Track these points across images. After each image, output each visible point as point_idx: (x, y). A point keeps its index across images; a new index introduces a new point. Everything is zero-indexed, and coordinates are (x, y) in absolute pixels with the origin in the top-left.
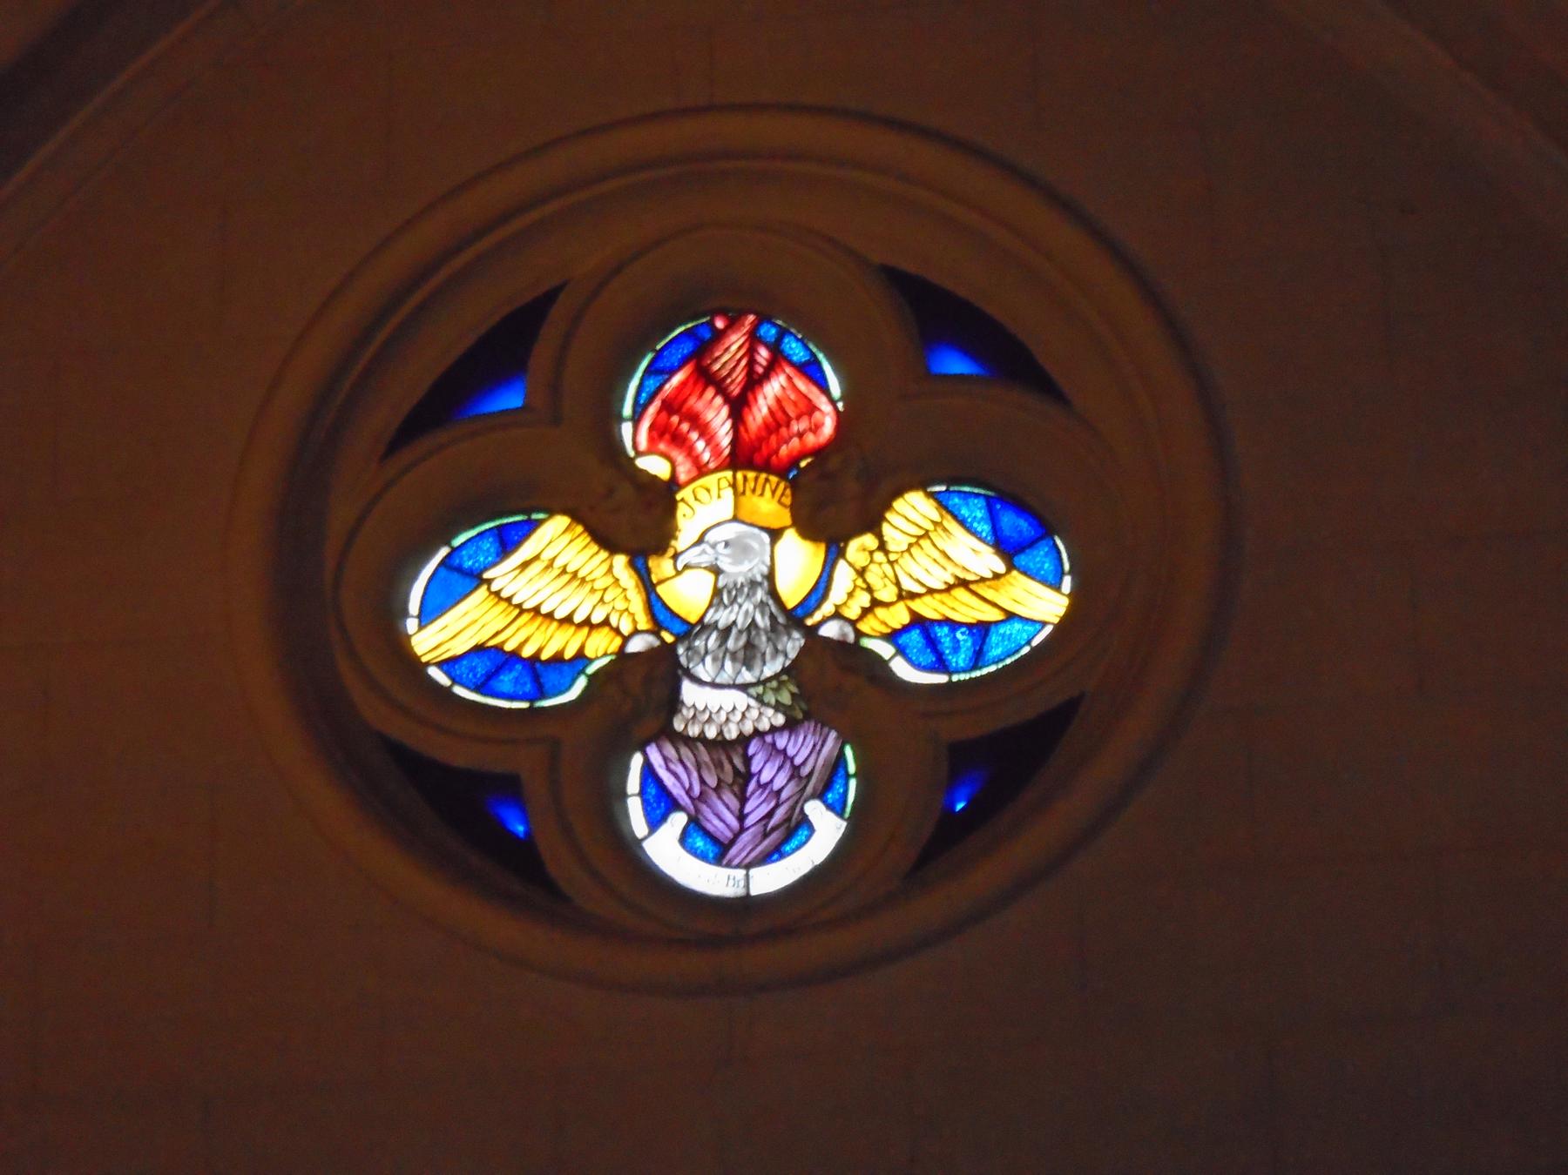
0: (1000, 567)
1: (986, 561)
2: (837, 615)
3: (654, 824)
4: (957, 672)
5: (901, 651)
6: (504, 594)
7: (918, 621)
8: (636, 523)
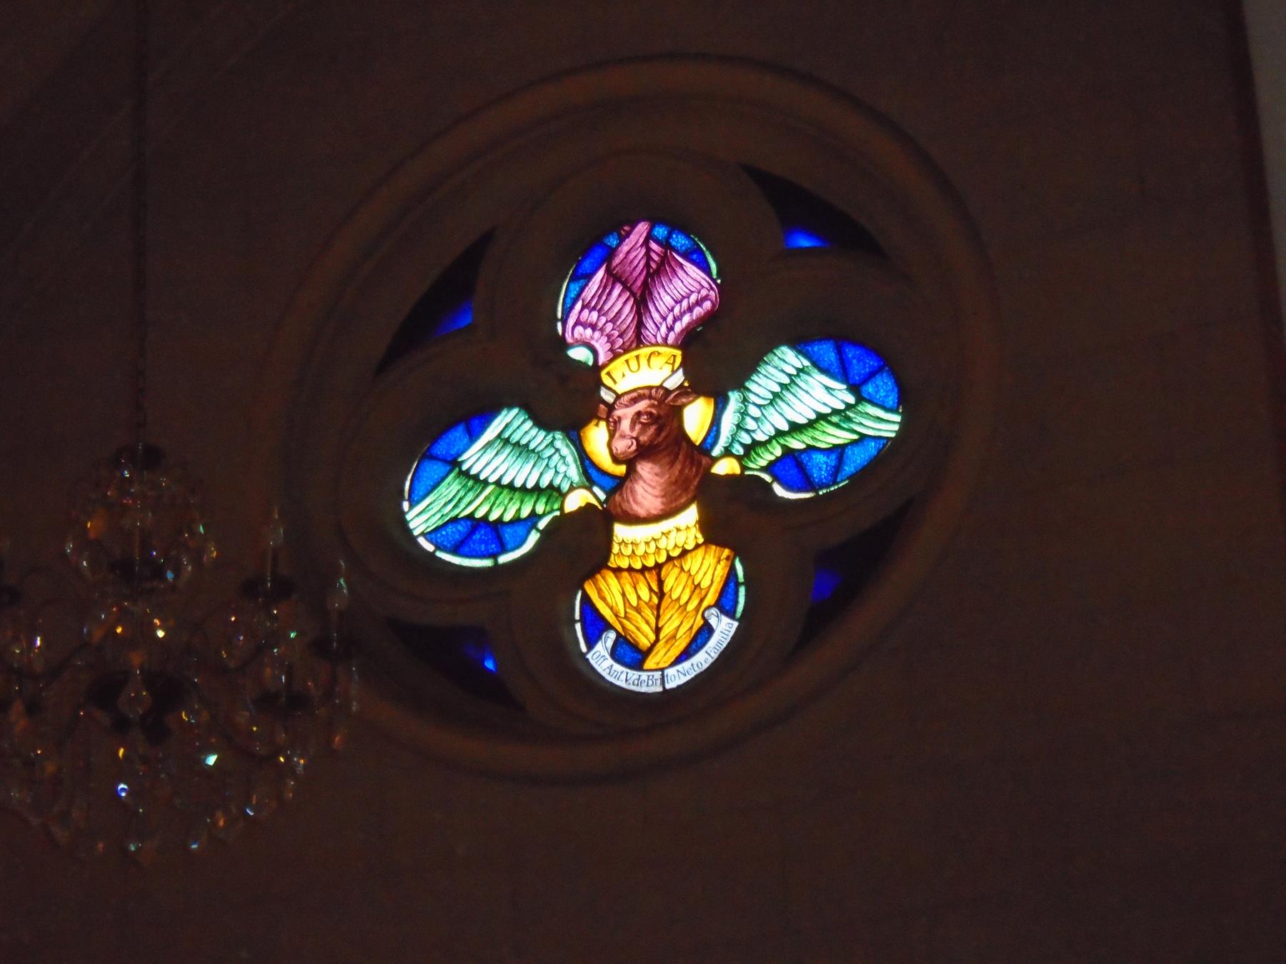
0: (851, 399)
1: (842, 396)
2: (727, 452)
3: (591, 646)
4: (821, 488)
5: (777, 478)
6: (518, 484)
7: (788, 453)
8: (568, 400)
